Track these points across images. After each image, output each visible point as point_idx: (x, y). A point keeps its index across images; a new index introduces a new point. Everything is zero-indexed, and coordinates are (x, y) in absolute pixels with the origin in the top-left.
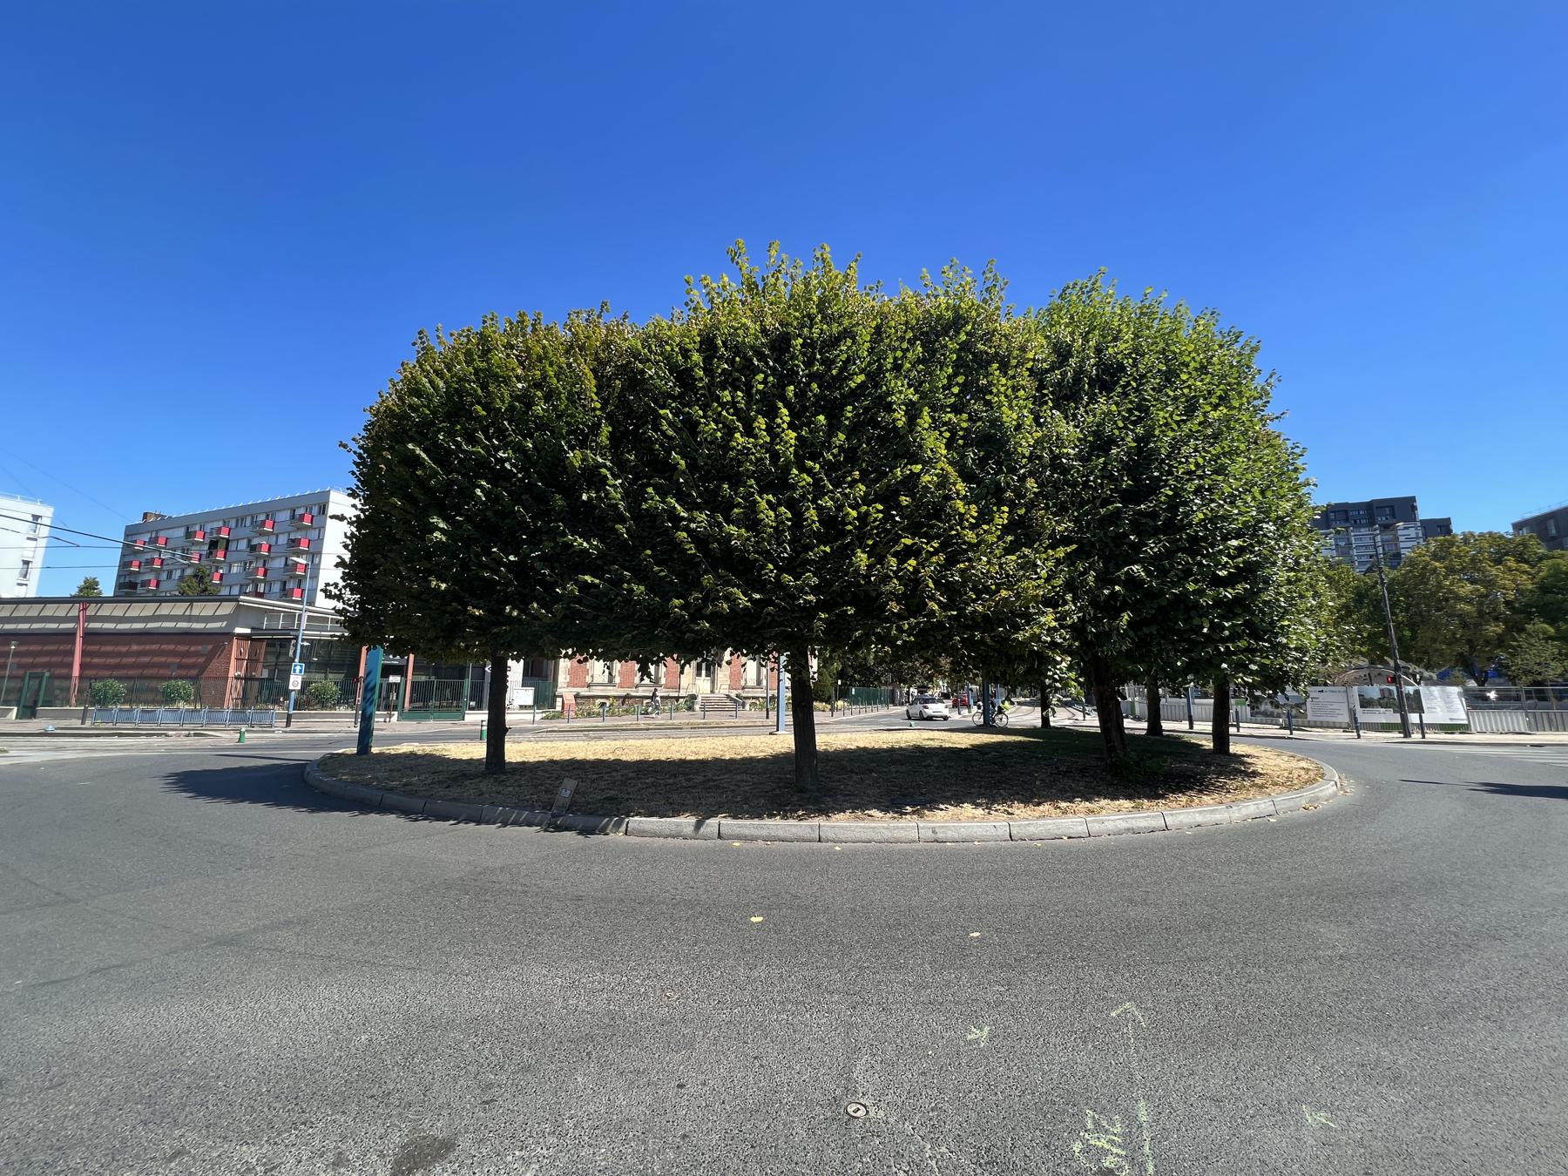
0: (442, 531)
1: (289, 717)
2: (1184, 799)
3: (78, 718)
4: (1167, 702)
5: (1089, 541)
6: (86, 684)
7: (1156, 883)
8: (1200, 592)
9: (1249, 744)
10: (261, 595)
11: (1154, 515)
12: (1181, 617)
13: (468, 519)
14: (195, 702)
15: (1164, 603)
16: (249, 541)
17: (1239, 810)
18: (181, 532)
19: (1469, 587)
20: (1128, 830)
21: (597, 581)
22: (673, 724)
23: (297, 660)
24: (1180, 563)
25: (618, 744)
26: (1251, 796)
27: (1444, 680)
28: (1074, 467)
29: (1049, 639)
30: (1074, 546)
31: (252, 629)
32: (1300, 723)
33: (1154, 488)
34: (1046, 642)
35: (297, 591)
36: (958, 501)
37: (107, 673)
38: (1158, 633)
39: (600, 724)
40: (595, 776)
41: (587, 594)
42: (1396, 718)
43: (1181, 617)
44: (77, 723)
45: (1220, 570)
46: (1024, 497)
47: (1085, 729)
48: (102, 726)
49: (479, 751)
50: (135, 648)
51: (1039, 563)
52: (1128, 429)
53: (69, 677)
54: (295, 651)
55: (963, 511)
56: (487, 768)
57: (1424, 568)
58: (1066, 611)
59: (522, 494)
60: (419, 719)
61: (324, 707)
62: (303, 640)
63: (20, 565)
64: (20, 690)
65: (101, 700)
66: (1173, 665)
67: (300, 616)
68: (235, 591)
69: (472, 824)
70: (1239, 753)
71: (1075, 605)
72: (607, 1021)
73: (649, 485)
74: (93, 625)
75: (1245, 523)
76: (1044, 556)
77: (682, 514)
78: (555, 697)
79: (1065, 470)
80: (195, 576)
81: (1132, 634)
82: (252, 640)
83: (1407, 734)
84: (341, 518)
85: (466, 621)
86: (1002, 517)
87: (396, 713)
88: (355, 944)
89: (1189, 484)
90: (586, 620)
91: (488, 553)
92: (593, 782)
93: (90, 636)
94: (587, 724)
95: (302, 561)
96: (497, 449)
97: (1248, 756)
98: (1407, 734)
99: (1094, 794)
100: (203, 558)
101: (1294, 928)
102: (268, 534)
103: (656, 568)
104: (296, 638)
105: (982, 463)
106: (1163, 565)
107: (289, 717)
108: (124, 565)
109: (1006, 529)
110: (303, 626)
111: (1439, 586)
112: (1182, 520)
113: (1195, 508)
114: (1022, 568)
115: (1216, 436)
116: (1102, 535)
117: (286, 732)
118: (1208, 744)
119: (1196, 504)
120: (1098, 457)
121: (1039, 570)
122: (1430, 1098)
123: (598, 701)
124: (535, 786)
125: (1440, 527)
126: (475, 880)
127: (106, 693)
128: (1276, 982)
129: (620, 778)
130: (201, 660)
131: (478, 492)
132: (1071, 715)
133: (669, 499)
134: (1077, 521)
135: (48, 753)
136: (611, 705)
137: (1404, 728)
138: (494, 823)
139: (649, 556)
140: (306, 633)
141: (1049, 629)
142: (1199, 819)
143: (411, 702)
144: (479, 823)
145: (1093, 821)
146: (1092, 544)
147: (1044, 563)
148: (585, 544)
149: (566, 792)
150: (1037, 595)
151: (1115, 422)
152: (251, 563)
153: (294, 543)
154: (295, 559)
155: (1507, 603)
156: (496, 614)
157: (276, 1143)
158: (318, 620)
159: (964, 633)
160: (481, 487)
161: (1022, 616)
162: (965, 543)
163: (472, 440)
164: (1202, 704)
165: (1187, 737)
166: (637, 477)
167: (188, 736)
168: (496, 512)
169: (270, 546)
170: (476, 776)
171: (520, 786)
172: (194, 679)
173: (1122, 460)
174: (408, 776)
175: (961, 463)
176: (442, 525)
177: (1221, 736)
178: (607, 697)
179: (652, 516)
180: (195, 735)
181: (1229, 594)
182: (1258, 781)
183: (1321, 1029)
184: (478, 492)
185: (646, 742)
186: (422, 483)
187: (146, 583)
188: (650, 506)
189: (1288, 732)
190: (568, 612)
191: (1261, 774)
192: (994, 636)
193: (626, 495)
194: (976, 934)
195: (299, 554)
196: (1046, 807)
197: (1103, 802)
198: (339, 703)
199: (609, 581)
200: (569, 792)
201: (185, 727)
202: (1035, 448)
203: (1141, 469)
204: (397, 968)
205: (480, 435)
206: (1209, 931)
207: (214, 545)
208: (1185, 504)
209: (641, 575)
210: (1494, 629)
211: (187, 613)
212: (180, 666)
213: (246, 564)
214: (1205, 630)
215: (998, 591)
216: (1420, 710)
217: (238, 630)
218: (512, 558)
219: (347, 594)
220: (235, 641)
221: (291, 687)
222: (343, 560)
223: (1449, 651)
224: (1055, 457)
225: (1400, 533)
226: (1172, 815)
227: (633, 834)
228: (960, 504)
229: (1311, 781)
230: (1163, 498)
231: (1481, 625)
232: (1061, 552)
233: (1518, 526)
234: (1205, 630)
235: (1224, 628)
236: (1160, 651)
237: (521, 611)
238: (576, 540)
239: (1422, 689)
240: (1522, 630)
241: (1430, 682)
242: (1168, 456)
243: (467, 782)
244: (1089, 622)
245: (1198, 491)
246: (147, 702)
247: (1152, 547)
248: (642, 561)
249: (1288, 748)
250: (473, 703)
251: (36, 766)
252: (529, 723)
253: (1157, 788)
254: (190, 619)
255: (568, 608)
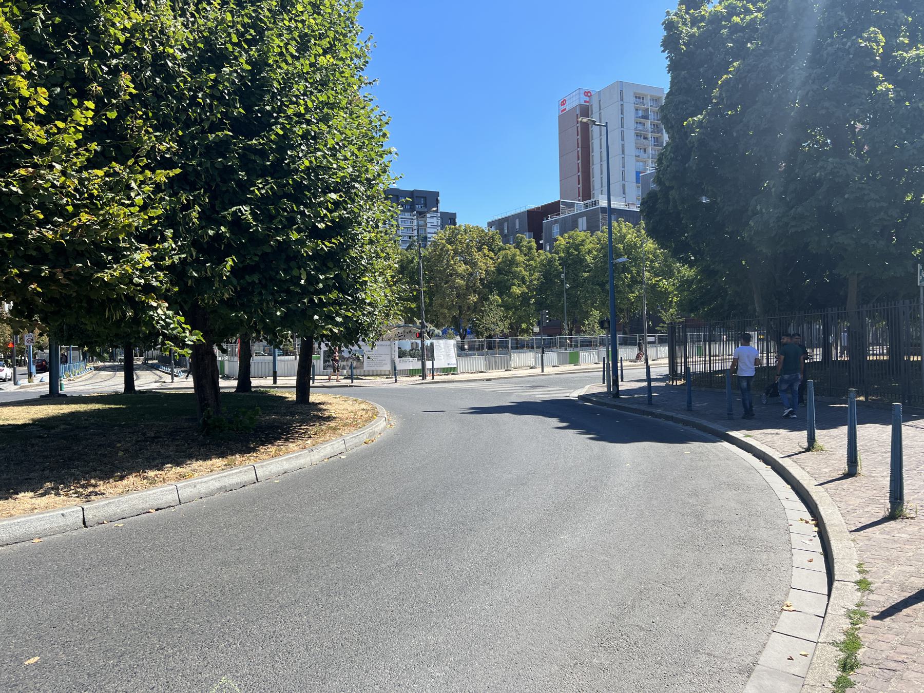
2: (272, 449)
4: (258, 361)
5: (195, 170)
7: (248, 538)
8: (300, 242)
9: (324, 393)
11: (263, 154)
12: (283, 266)
15: (269, 250)
17: (319, 452)
19: (464, 267)
20: (221, 488)
24: (285, 210)
26: (328, 438)
27: (445, 336)
28: (180, 74)
29: (142, 281)
30: (178, 171)
32: (358, 374)
33: (265, 124)
34: (139, 285)
36: (19, 78)
38: (260, 282)
42: (419, 366)
43: (283, 266)
45: (319, 222)
46: (116, 96)
47: (173, 392)
51: (133, 185)
52: (241, 47)
55: (25, 93)
57: (442, 249)
58: (165, 249)
66: (272, 316)
70: (317, 402)
71: (176, 243)
75: (343, 178)
76: (140, 177)
79: (170, 77)
81: (235, 281)
83: (424, 377)
86: (84, 116)
89: (298, 127)
97: (323, 404)
98: (424, 377)
99: (186, 457)
101: (363, 549)
105: (59, 33)
106: (269, 210)
109: (90, 134)
111: (448, 265)
112: (288, 164)
113: (301, 155)
114: (111, 190)
115: (324, 83)
116: (208, 165)
118: (292, 396)
119: (302, 150)
120: (209, 71)
121: (133, 194)
122: (459, 662)
125: (450, 219)
128: (353, 604)
132: (157, 378)
134: (180, 141)
137: (422, 373)
141: (143, 270)
142: (286, 466)
145: (185, 487)
146: (198, 174)
147: (139, 187)
150: (130, 225)
151: (229, 35)
155: (481, 280)
159: (24, 267)
161: (109, 250)
162: (28, 141)
164: (284, 361)
165: (273, 392)
173: (233, 83)
175: (26, 25)
177: (303, 388)
181: (325, 246)
182: (333, 424)
183: (387, 634)
189: (350, 381)
191: (334, 418)
192: (69, 273)
194: (32, 661)
196: (131, 480)
197: (196, 465)
202: (132, 36)
203: (253, 99)
206: (297, 573)
208: (292, 148)
210: (473, 298)
214: (302, 282)
215: (76, 214)
216: (432, 358)
223: (448, 314)
224: (159, 57)
225: (428, 220)
226: (262, 466)
228: (22, 84)
229: (369, 419)
230: (273, 137)
231: (467, 296)
232: (161, 176)
233: (490, 224)
234: (302, 282)
235: (318, 281)
236: (261, 302)
239: (435, 342)
240: (487, 299)
241: (438, 337)
242: (280, 92)
244: (191, 264)
245: (305, 136)
247: (260, 188)
249: (350, 394)
253: (248, 442)
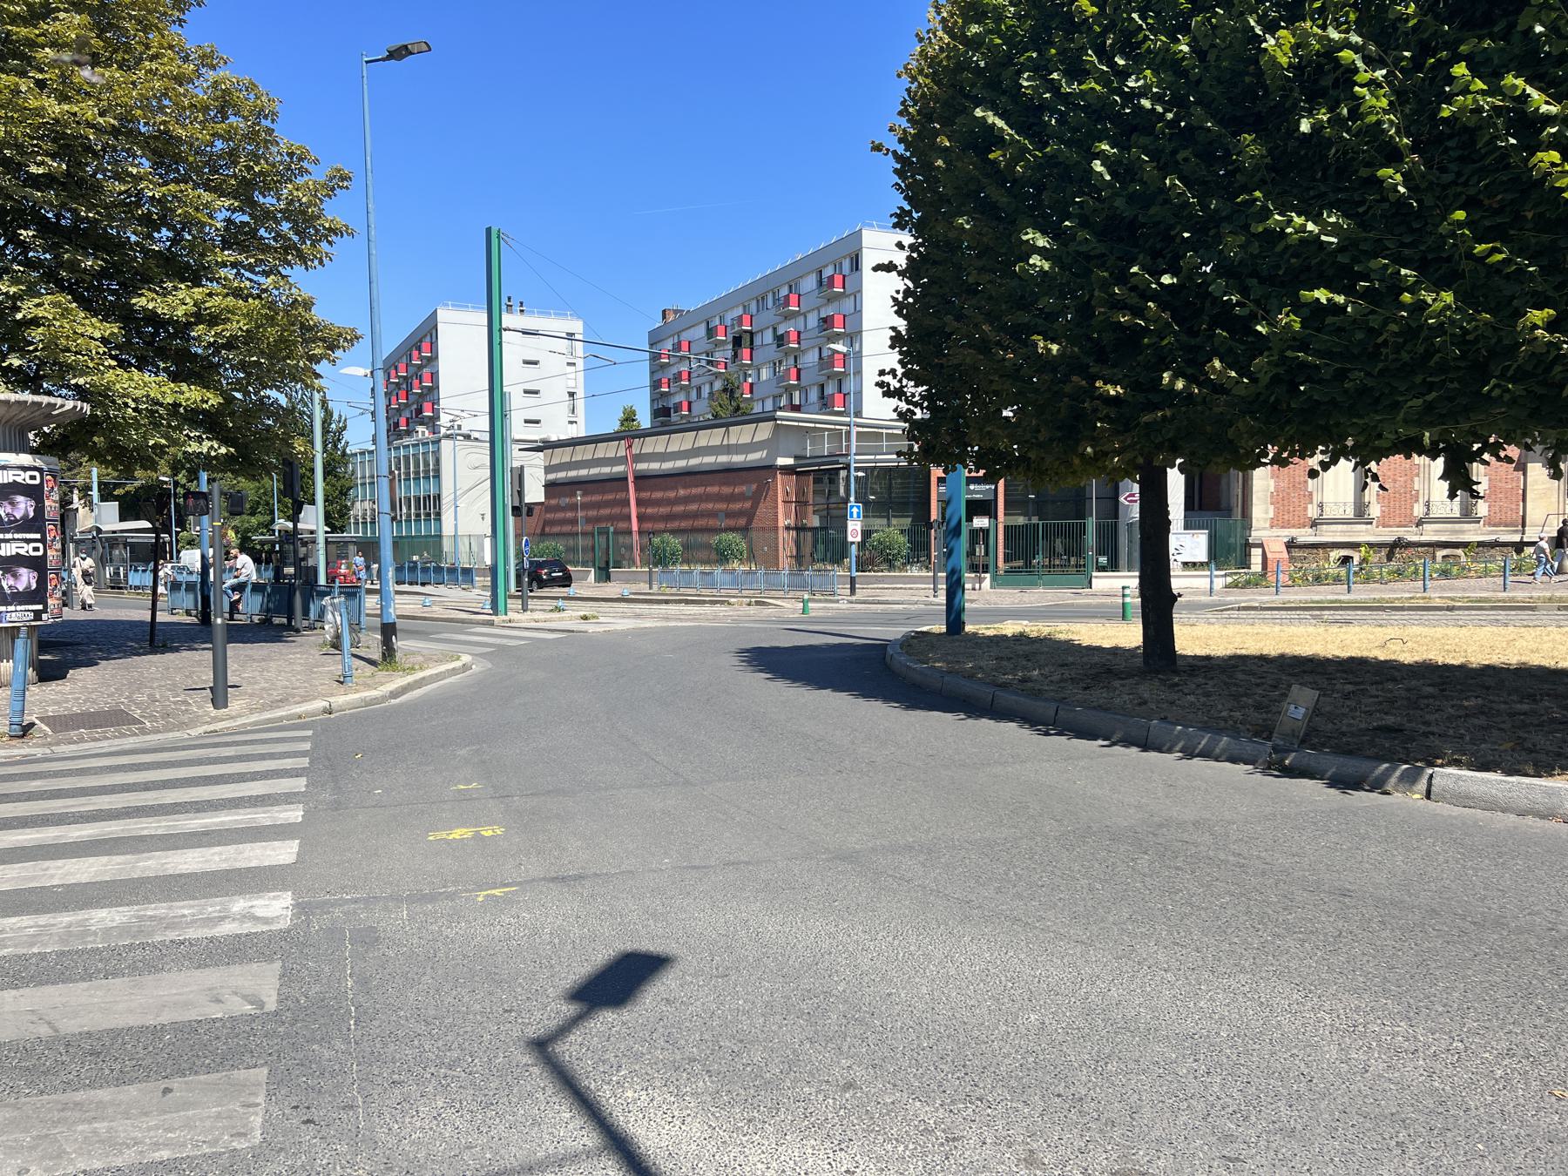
0: (1042, 252)
1: (853, 581)
3: (645, 582)
6: (646, 540)
10: (797, 408)
13: (1084, 222)
14: (749, 560)
16: (775, 329)
18: (701, 331)
21: (1340, 299)
22: (1512, 600)
23: (852, 499)
25: (1391, 632)
31: (796, 457)
35: (838, 398)
37: (661, 526)
39: (1342, 597)
40: (1350, 688)
41: (1319, 330)
44: (644, 587)
48: (668, 591)
49: (1131, 635)
50: (682, 492)
53: (630, 533)
54: (848, 485)
56: (1146, 662)
59: (1174, 152)
60: (1023, 585)
61: (891, 567)
62: (857, 469)
63: (567, 397)
64: (593, 548)
65: (660, 559)
67: (848, 433)
68: (769, 406)
69: (1134, 750)
72: (1430, 1103)
73: (1456, 59)
74: (642, 466)
77: (1544, 108)
78: (1247, 546)
80: (725, 390)
82: (798, 474)
84: (889, 267)
85: (1095, 410)
87: (988, 575)
88: (998, 891)
90: (1320, 381)
91: (1123, 278)
92: (1347, 696)
93: (641, 478)
94: (1317, 598)
95: (840, 347)
96: (1123, 74)
100: (729, 365)
102: (794, 315)
103: (1480, 248)
104: (847, 467)
107: (853, 581)
108: (656, 385)
110: (854, 450)
117: (852, 602)
123: (1335, 554)
124: (1236, 697)
126: (1155, 835)
127: (664, 550)
129: (1404, 693)
130: (748, 505)
131: (1098, 166)
133: (1509, 80)
135: (626, 621)
136: (1364, 560)
138: (1169, 751)
139: (1460, 224)
140: (859, 460)
143: (1006, 560)
144: (1145, 747)
148: (1310, 226)
149: (1298, 707)
152: (780, 362)
153: (826, 322)
154: (832, 346)
156: (1147, 390)
157: (951, 1111)
158: (872, 436)
160: (1097, 156)
163: (1077, 71)
166: (1424, 50)
167: (749, 605)
168: (1132, 199)
169: (799, 333)
170: (1130, 675)
171: (1207, 695)
172: (745, 530)
174: (1024, 668)
176: (1042, 242)
178: (1355, 546)
179: (1467, 131)
180: (758, 603)
184: (1098, 166)
185: (1452, 631)
186: (998, 175)
187: (678, 407)
188: (1462, 109)
190: (1281, 370)
193: (1400, 98)
195: (836, 338)
198: (909, 561)
199: (1366, 294)
200: (1302, 710)
201: (745, 593)
204: (1061, 936)
205: (1091, 56)
207: (737, 342)
209: (1438, 271)
211: (725, 443)
212: (729, 515)
213: (775, 364)
217: (781, 461)
218: (1166, 280)
219: (910, 388)
220: (779, 476)
221: (850, 539)
222: (898, 333)
227: (1443, 799)
237: (1191, 379)
238: (1290, 222)
243: (1117, 683)
246: (703, 562)
248: (1443, 238)
250: (1103, 560)
251: (625, 633)
252: (1204, 594)
254: (729, 449)
255: (1283, 359)
